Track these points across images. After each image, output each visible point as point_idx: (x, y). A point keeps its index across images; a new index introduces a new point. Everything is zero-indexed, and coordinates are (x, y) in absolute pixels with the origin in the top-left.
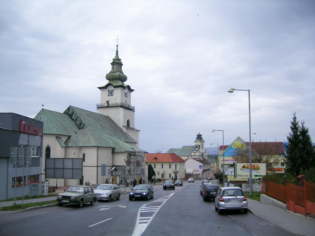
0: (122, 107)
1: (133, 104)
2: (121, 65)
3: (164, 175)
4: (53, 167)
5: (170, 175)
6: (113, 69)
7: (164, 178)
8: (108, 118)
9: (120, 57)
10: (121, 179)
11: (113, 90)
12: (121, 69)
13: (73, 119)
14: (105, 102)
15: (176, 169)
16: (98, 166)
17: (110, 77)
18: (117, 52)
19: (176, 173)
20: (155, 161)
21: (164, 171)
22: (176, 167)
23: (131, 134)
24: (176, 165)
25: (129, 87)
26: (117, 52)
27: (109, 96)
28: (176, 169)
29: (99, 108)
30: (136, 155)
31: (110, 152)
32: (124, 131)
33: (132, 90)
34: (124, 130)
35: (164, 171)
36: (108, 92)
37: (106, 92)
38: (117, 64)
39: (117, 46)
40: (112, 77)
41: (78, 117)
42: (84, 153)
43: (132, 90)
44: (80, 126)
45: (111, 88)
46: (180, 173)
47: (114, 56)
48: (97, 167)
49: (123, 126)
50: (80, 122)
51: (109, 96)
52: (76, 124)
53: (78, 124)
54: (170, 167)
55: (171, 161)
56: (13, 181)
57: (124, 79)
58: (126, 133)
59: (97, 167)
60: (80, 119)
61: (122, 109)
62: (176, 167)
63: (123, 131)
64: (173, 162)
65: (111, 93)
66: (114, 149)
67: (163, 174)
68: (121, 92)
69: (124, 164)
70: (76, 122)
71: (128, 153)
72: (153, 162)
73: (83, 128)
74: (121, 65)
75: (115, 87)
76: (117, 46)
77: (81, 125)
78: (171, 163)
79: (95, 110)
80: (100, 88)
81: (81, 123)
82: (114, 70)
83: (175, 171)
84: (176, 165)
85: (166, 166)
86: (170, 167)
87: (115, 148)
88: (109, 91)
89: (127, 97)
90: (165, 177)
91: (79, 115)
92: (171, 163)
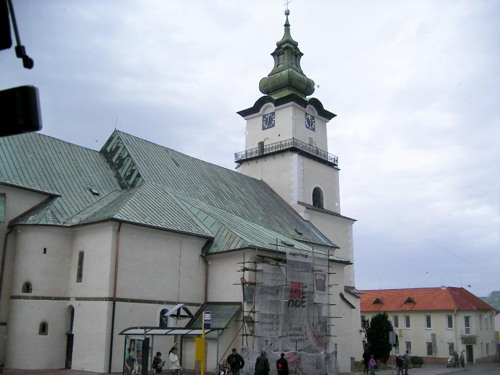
0: (293, 150)
1: (332, 151)
2: (298, 55)
3: (435, 345)
4: (105, 306)
5: (451, 346)
6: (277, 65)
7: (433, 355)
8: (262, 184)
9: (294, 37)
10: (129, 350)
11: (273, 113)
12: (298, 66)
13: (112, 165)
14: (256, 146)
15: (468, 331)
16: (118, 296)
17: (268, 85)
18: (287, 25)
19: (469, 343)
20: (407, 307)
21: (434, 336)
22: (467, 322)
23: (319, 222)
24: (467, 319)
25: (316, 103)
26: (287, 25)
27: (264, 129)
28: (468, 331)
29: (240, 162)
30: (285, 261)
31: (192, 253)
32: (302, 214)
33: (330, 116)
34: (302, 212)
35: (434, 336)
36: (263, 121)
37: (258, 120)
38: (286, 52)
39: (287, 14)
40: (272, 83)
41: (129, 155)
42: (81, 249)
43: (330, 116)
44: (126, 180)
45: (269, 108)
46: (482, 343)
47: (280, 36)
48: (110, 299)
49: (299, 203)
50: (130, 169)
51: (264, 129)
52: (118, 176)
53: (122, 176)
54: (450, 325)
55: (453, 306)
56: (152, 347)
57: (309, 87)
58: (308, 221)
59: (110, 299)
60: (132, 161)
61: (295, 157)
62: (467, 322)
63: (297, 217)
64: (459, 310)
65: (269, 122)
66: (209, 241)
67: (431, 344)
68: (294, 114)
69: (236, 295)
70: (120, 171)
71: (257, 253)
72: (402, 311)
73: (133, 185)
74: (296, 56)
75: (278, 103)
76: (287, 14)
77: (129, 177)
78: (452, 311)
79: (232, 166)
80: (244, 113)
81: (133, 171)
82: (280, 66)
83: (464, 334)
84: (467, 319)
85: (439, 321)
86: (450, 325)
87: (216, 240)
88: (264, 116)
89: (314, 130)
90: (436, 352)
91: (131, 153)
92: (452, 311)
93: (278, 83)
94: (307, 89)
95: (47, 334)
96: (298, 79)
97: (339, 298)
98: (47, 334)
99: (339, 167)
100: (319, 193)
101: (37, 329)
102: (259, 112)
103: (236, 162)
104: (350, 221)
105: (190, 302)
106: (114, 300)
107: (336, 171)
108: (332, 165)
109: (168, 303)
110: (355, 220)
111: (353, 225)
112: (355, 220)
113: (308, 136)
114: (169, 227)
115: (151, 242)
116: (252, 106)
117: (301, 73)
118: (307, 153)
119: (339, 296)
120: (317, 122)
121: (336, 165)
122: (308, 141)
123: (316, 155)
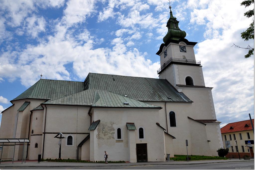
16: (46, 131)
33: (194, 44)
61: (175, 66)
74: (176, 23)
93: (168, 37)
94: (181, 35)
95: (37, 148)
96: (175, 33)
97: (156, 125)
98: (37, 148)
99: (202, 65)
100: (190, 79)
101: (34, 146)
102: (162, 51)
103: (158, 74)
104: (211, 89)
105: (83, 132)
106: (45, 133)
107: (200, 67)
108: (199, 65)
109: (72, 133)
110: (212, 88)
111: (212, 90)
112: (212, 88)
113: (182, 55)
114: (155, 106)
115: (237, 116)
116: (189, 41)
117: (179, 30)
118: (168, 65)
119: (156, 125)
120: (188, 48)
121: (200, 65)
122: (182, 57)
123: (186, 62)
